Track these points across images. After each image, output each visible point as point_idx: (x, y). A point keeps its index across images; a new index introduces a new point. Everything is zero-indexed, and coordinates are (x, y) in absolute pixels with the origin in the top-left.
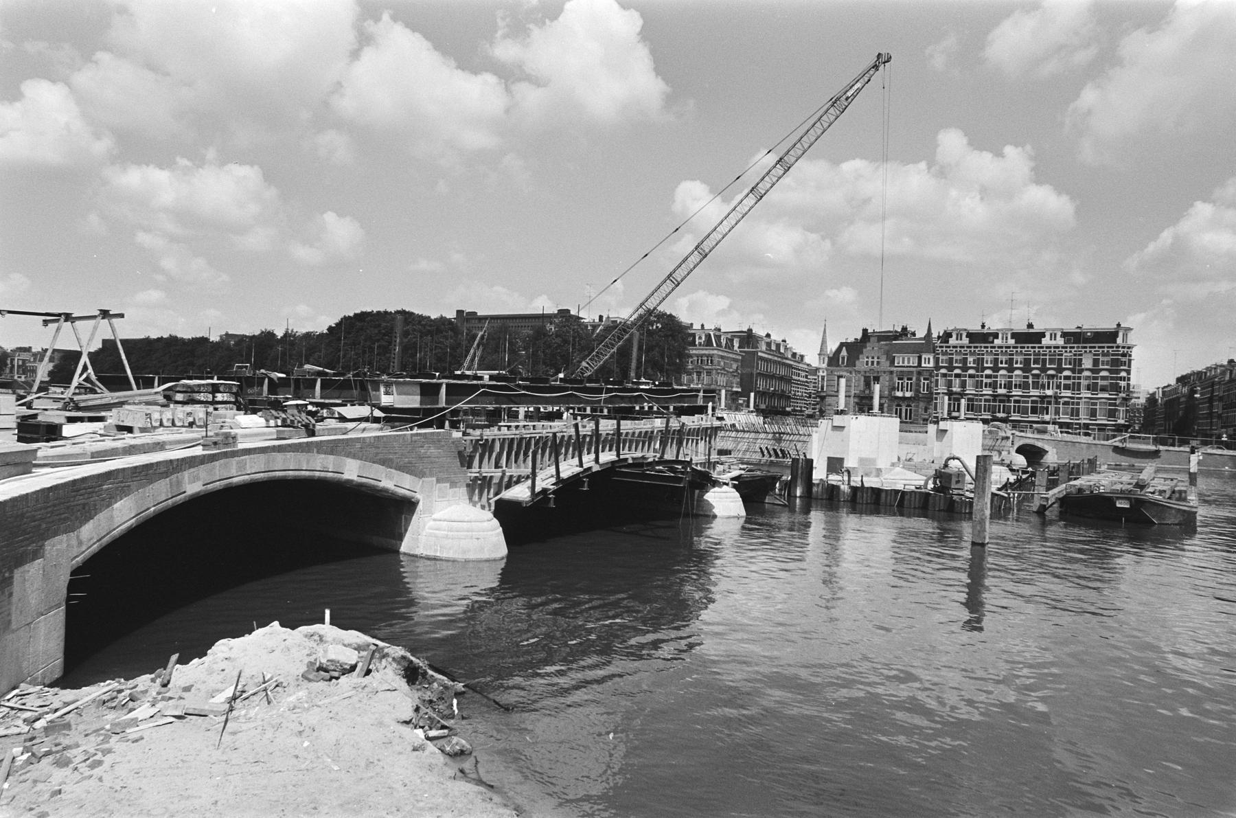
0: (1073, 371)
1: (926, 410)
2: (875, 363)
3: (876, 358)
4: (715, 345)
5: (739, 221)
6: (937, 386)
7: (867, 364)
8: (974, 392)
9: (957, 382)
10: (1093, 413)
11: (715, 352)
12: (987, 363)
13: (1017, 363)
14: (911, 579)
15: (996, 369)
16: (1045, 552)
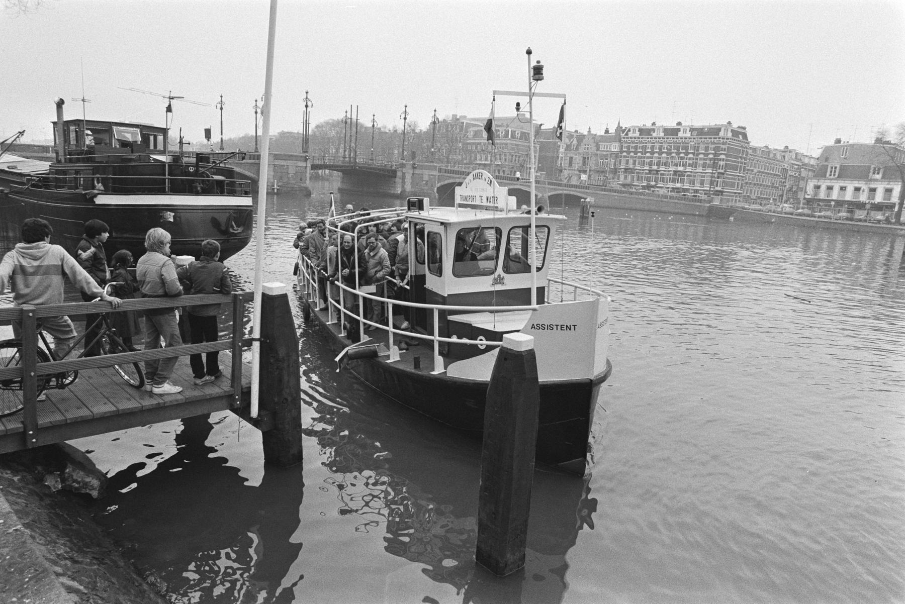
0: (693, 154)
4: (510, 137)
5: (256, 144)
6: (620, 163)
8: (701, 171)
9: (631, 161)
10: (702, 183)
15: (660, 153)
16: (842, 308)
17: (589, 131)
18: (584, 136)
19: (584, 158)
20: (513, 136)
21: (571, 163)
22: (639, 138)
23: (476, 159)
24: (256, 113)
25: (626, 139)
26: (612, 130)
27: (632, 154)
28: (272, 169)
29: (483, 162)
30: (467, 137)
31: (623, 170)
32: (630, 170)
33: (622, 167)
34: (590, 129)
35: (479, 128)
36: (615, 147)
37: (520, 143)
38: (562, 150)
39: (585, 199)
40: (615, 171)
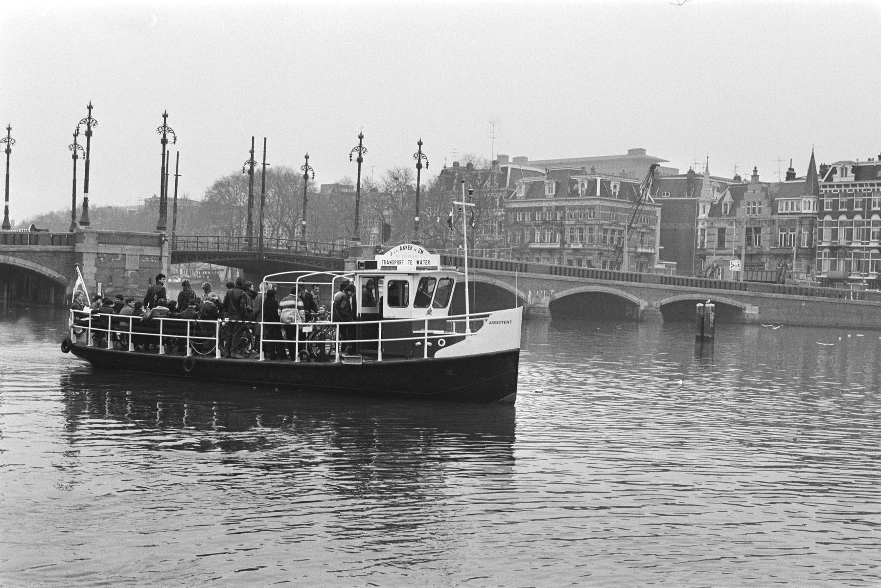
1: (809, 269)
2: (757, 210)
3: (757, 204)
4: (598, 193)
6: (821, 238)
7: (754, 213)
9: (842, 233)
11: (597, 202)
12: (875, 206)
13: (875, 206)
14: (740, 496)
17: (755, 176)
18: (745, 187)
19: (748, 230)
20: (605, 191)
21: (721, 242)
22: (854, 185)
23: (532, 241)
24: (75, 157)
25: (828, 189)
26: (801, 172)
27: (843, 218)
28: (93, 262)
29: (548, 246)
30: (515, 197)
31: (827, 250)
32: (841, 251)
33: (824, 245)
34: (755, 171)
35: (537, 179)
36: (807, 206)
37: (620, 205)
38: (702, 215)
39: (704, 302)
40: (811, 253)
